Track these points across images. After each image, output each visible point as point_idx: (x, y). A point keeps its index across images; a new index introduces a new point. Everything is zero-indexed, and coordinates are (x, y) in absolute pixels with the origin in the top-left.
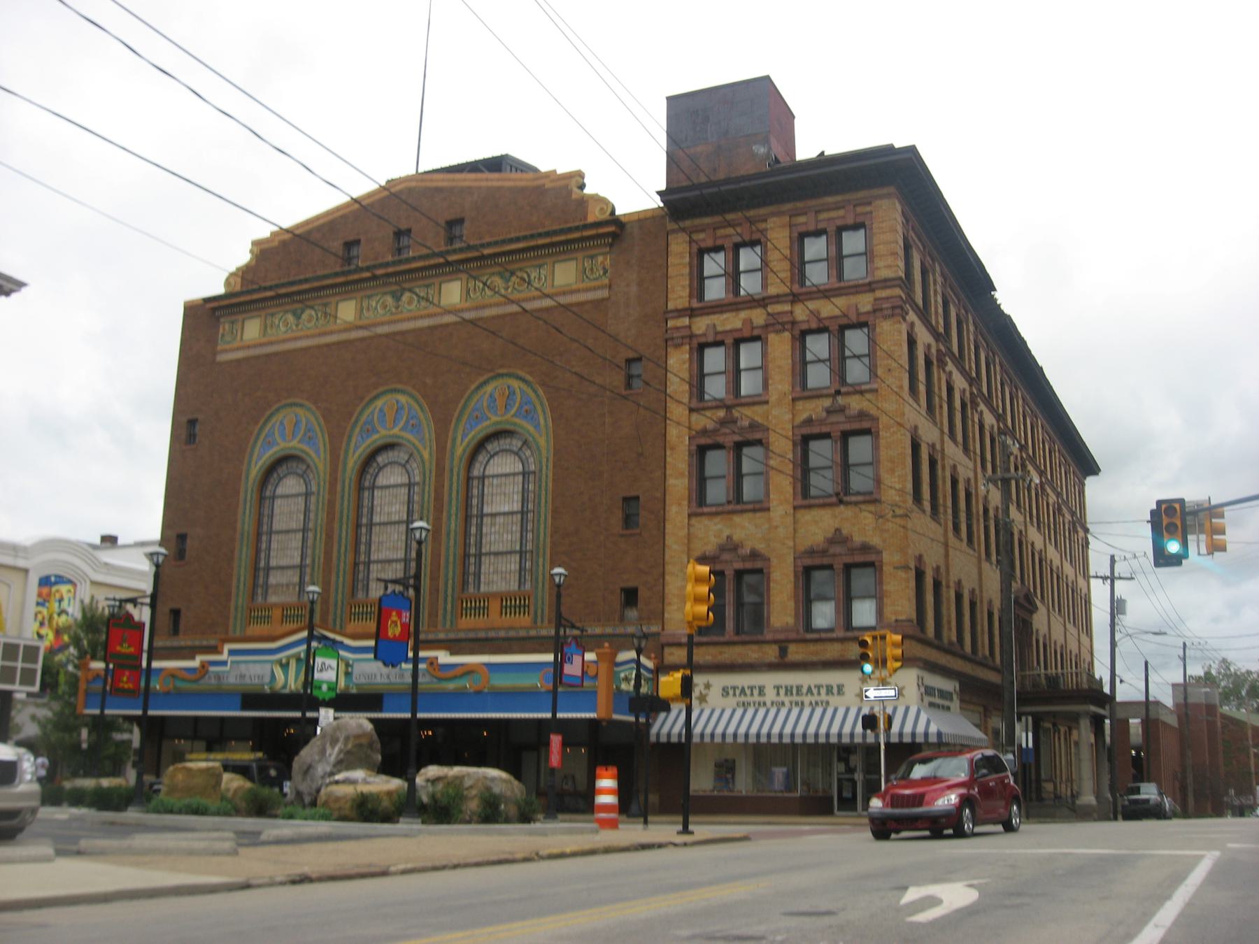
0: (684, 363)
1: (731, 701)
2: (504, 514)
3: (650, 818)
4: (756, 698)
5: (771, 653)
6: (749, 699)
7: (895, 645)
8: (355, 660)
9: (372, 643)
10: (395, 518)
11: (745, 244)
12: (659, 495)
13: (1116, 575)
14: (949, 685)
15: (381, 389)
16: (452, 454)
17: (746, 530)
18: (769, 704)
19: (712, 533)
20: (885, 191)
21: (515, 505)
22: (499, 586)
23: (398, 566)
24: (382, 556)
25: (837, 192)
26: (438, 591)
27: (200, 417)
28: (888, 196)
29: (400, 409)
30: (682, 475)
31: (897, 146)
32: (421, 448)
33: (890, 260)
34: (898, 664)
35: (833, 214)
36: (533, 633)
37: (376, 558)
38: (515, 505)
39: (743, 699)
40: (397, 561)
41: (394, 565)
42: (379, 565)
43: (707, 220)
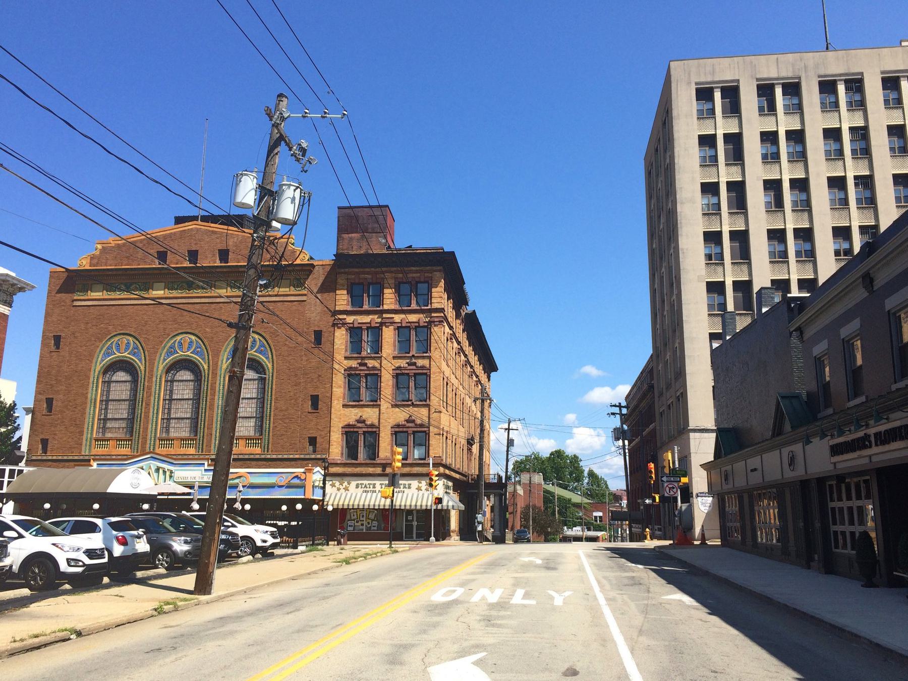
0: (343, 335)
1: (360, 490)
2: (248, 398)
3: (330, 543)
4: (371, 489)
5: (379, 470)
6: (368, 489)
7: (398, 461)
8: (175, 470)
9: (667, 504)
10: (186, 397)
11: (372, 283)
12: (329, 395)
13: (511, 428)
14: (450, 484)
15: (180, 331)
16: (221, 368)
17: (370, 415)
18: (377, 492)
19: (352, 415)
20: (439, 268)
21: (254, 394)
22: (246, 433)
23: (187, 421)
24: (178, 416)
25: (417, 266)
26: (211, 434)
27: (63, 335)
28: (440, 271)
29: (191, 342)
30: (340, 387)
31: (465, 286)
32: (203, 363)
33: (439, 300)
34: (437, 478)
35: (414, 275)
36: (263, 457)
37: (174, 416)
38: (254, 394)
39: (365, 489)
40: (187, 418)
41: (185, 421)
42: (176, 421)
43: (356, 270)
